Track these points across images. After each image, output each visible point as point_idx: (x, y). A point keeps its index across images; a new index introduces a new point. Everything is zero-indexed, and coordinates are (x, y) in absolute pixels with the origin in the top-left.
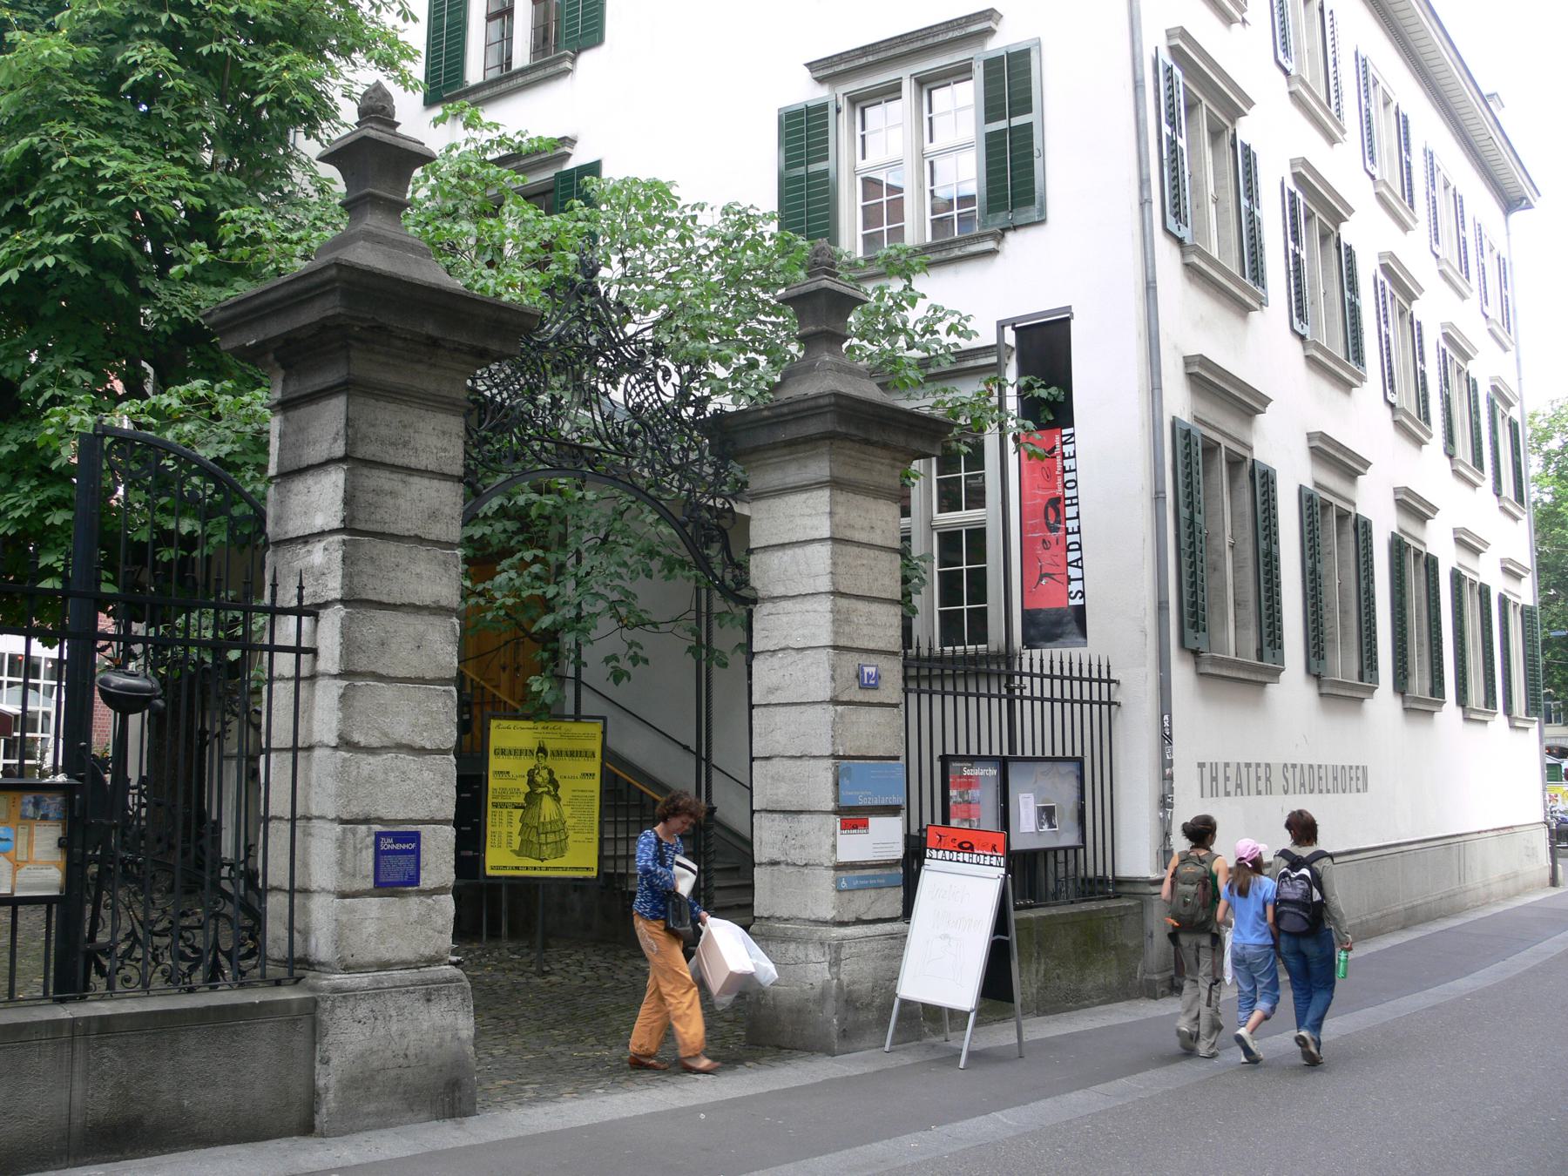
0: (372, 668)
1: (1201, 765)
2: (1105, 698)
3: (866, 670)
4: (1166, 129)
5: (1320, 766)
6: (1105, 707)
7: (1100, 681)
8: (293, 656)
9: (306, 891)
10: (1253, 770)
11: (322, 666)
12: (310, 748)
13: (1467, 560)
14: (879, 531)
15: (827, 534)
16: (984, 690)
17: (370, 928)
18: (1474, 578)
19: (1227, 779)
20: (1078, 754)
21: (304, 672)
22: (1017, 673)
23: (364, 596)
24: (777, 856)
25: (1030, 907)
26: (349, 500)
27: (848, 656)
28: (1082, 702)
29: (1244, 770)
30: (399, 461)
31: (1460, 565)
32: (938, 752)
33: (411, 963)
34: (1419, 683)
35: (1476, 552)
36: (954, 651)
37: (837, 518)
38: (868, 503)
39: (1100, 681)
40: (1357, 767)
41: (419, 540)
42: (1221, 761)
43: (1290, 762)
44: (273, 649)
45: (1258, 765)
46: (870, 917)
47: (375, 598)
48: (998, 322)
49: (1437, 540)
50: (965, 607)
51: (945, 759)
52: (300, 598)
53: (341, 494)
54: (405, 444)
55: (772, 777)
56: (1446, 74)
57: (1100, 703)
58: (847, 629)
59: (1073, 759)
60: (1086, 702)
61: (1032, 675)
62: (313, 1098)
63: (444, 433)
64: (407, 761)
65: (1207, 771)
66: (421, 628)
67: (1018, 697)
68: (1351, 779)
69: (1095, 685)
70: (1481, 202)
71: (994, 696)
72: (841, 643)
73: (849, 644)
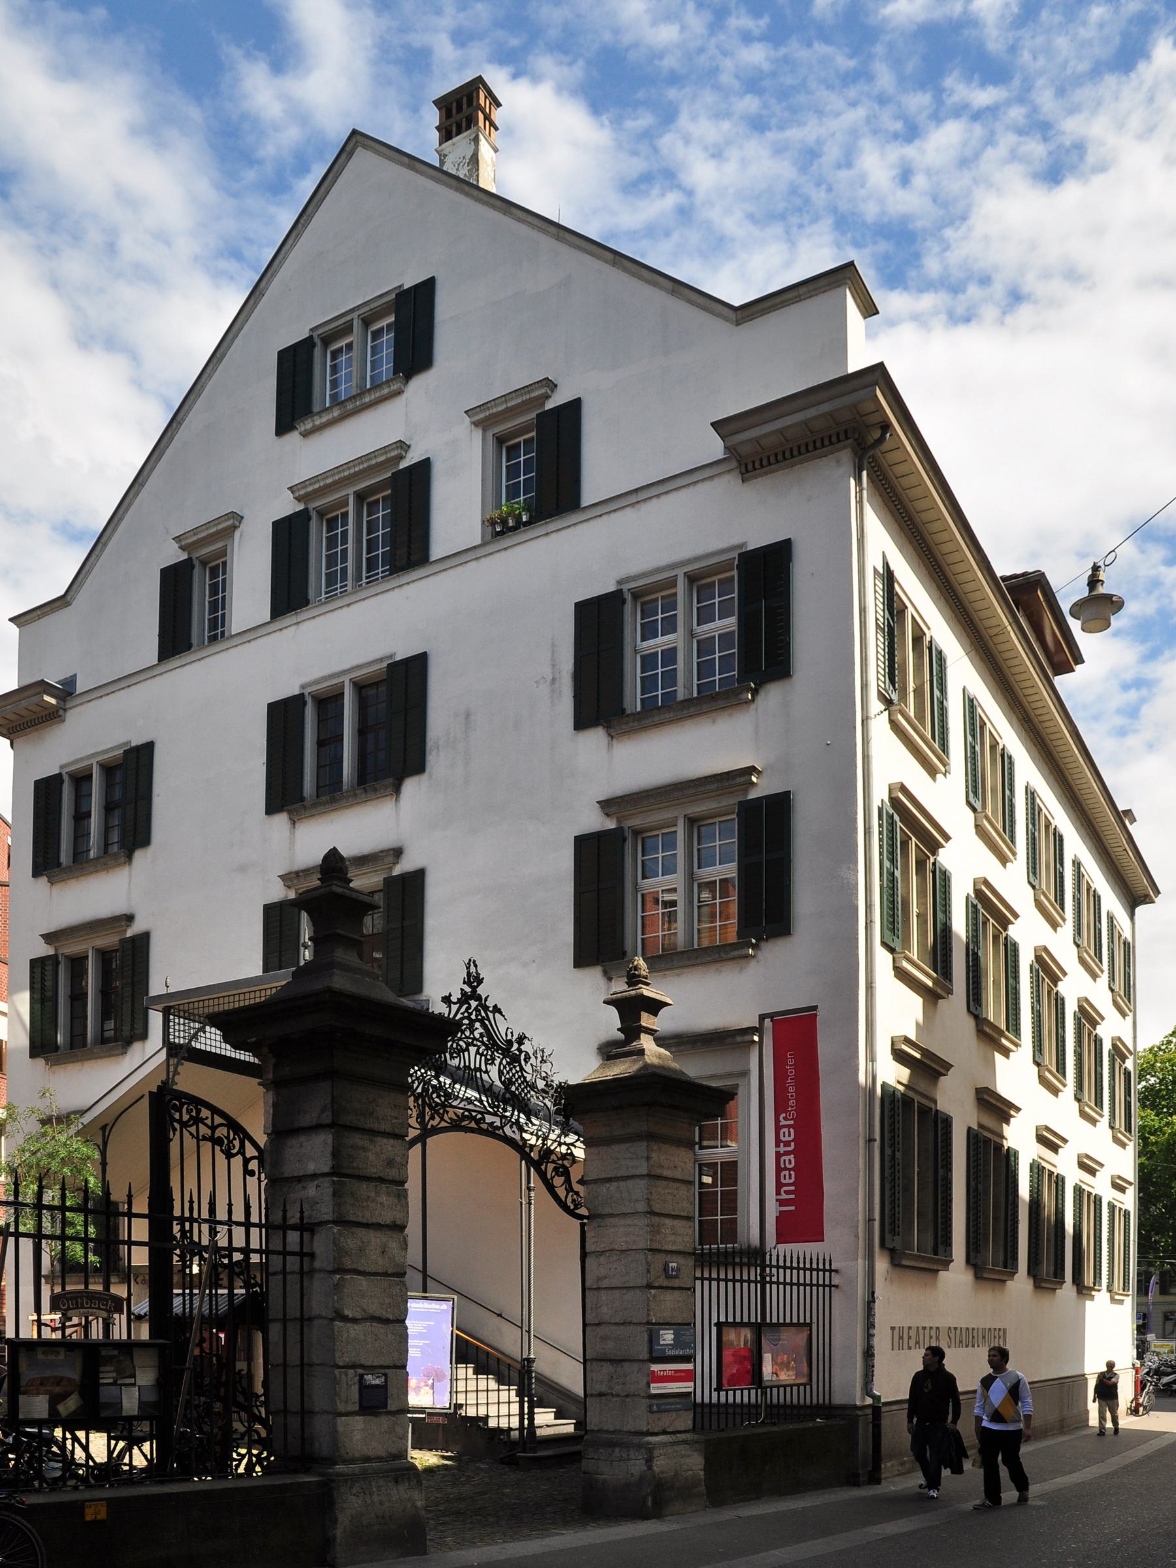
0: (354, 1266)
1: (893, 1329)
2: (827, 1282)
3: (671, 1265)
4: (887, 864)
5: (973, 1329)
6: (827, 1289)
8: (298, 1258)
9: (312, 1413)
10: (927, 1331)
11: (317, 1264)
12: (310, 1319)
13: (1086, 1177)
14: (680, 1170)
15: (645, 1172)
17: (357, 1436)
18: (1091, 1190)
19: (909, 1338)
20: (808, 1321)
21: (306, 1269)
22: (768, 1266)
23: (348, 1218)
24: (604, 1389)
26: (335, 1154)
27: (659, 1256)
29: (921, 1331)
30: (367, 1126)
31: (1081, 1181)
32: (714, 1320)
33: (383, 1458)
34: (1046, 1267)
35: (1054, 1148)
36: (710, 1248)
37: (652, 1162)
39: (824, 1270)
41: (381, 1180)
42: (906, 1325)
43: (952, 1326)
44: (130, 1243)
45: (931, 1328)
47: (355, 1220)
49: (1064, 1164)
50: (719, 1217)
51: (719, 1325)
53: (330, 1149)
58: (658, 1237)
59: (805, 1324)
61: (778, 1267)
63: (395, 1106)
64: (378, 1328)
65: (896, 1332)
66: (384, 1240)
67: (768, 1282)
68: (995, 1337)
70: (1111, 902)
72: (655, 1246)
73: (659, 1247)
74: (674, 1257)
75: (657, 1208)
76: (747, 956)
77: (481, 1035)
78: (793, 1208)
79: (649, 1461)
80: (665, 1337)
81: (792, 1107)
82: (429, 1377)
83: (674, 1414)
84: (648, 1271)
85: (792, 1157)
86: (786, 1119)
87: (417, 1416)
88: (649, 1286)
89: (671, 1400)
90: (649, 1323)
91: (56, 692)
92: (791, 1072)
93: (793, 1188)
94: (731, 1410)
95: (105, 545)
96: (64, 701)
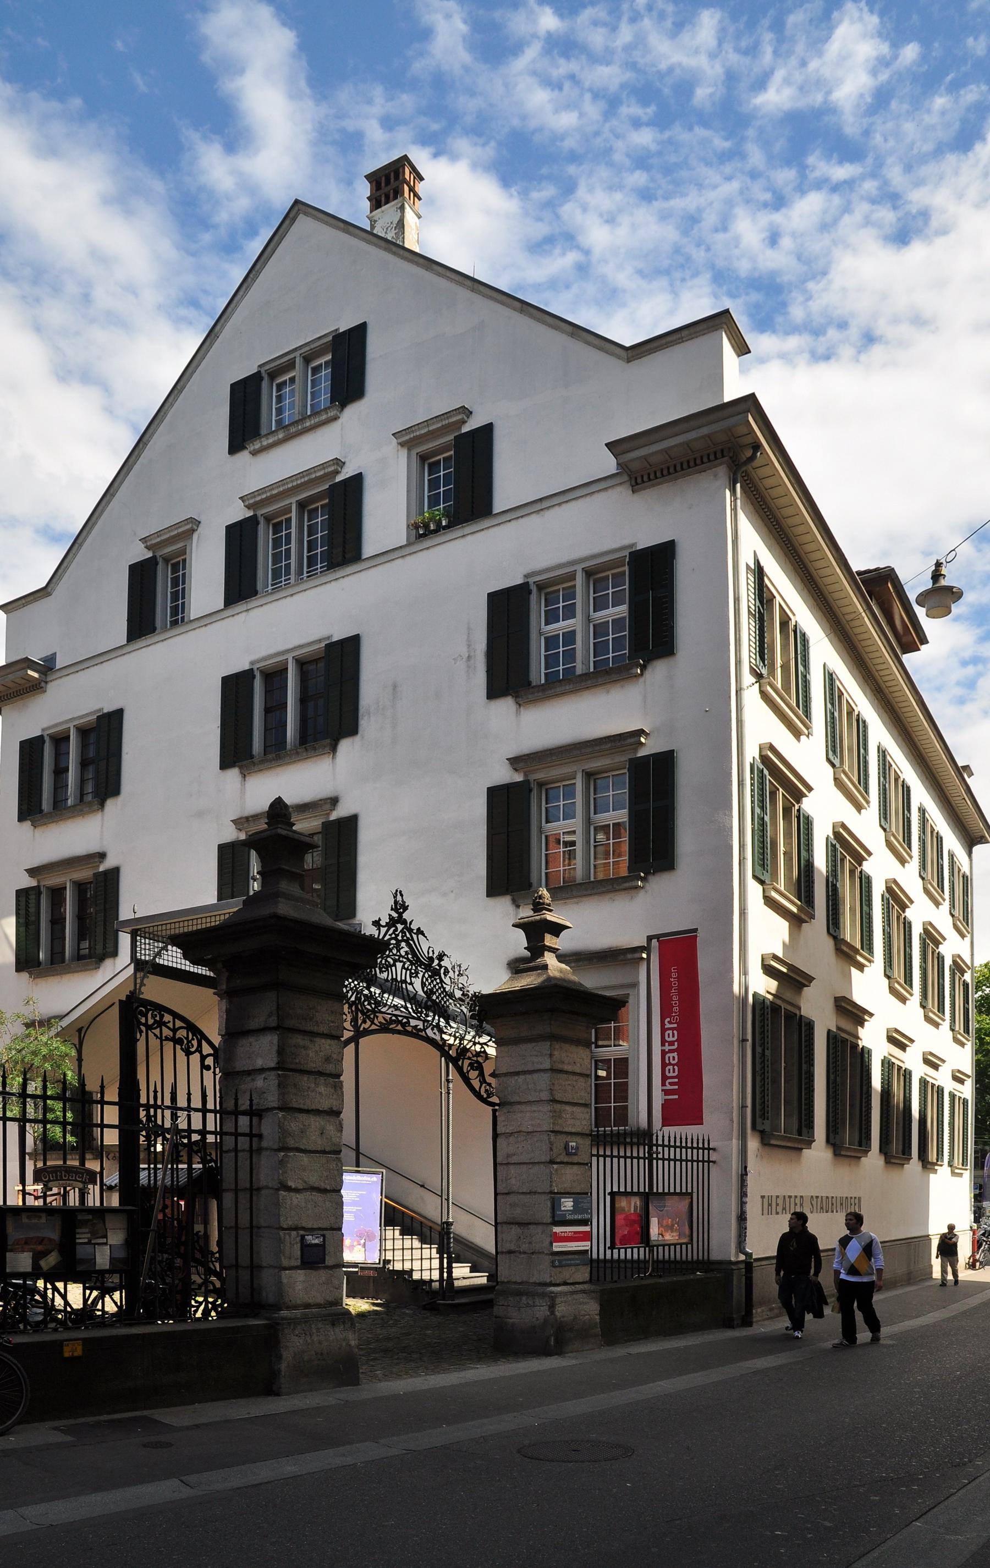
0: (297, 1145)
1: (763, 1197)
2: (706, 1159)
3: (570, 1144)
4: (758, 810)
5: (833, 1197)
6: (706, 1164)
7: (703, 1149)
10: (792, 1200)
11: (265, 1144)
12: (259, 1189)
14: (578, 1065)
16: (608, 1153)
17: (299, 1287)
18: (934, 1082)
19: (777, 1205)
20: (689, 1191)
21: (255, 1147)
22: (655, 1145)
24: (513, 1247)
25: (660, 1277)
26: (281, 1052)
28: (687, 1161)
29: (787, 1200)
31: (926, 1074)
32: (608, 1190)
33: (321, 1305)
34: (895, 1146)
35: (903, 1047)
38: (573, 1048)
39: (703, 1149)
40: (855, 1198)
41: (320, 1074)
42: (774, 1194)
45: (796, 1197)
46: (571, 1281)
47: (297, 1106)
48: (648, 937)
49: (911, 1060)
51: (612, 1194)
52: (236, 1105)
53: (275, 1048)
54: (311, 1019)
55: (510, 1204)
56: (937, 758)
57: (703, 1161)
58: (560, 1121)
59: (687, 1194)
60: (700, 1161)
62: (274, 1375)
64: (316, 1196)
65: (766, 1200)
67: (655, 1159)
69: (701, 1151)
71: (608, 1156)
72: (557, 1128)
73: (561, 1129)
74: (574, 1138)
75: (558, 1096)
76: (637, 887)
77: (407, 953)
78: (676, 1097)
79: (552, 1307)
80: (566, 1204)
81: (676, 1013)
82: (361, 1238)
83: (573, 1268)
84: (551, 1149)
85: (675, 1054)
86: (670, 1023)
87: (351, 1269)
88: (552, 1162)
89: (570, 1257)
90: (551, 1192)
91: (38, 667)
92: (675, 984)
93: (676, 1080)
94: (622, 1265)
95: (81, 545)
96: (46, 675)
